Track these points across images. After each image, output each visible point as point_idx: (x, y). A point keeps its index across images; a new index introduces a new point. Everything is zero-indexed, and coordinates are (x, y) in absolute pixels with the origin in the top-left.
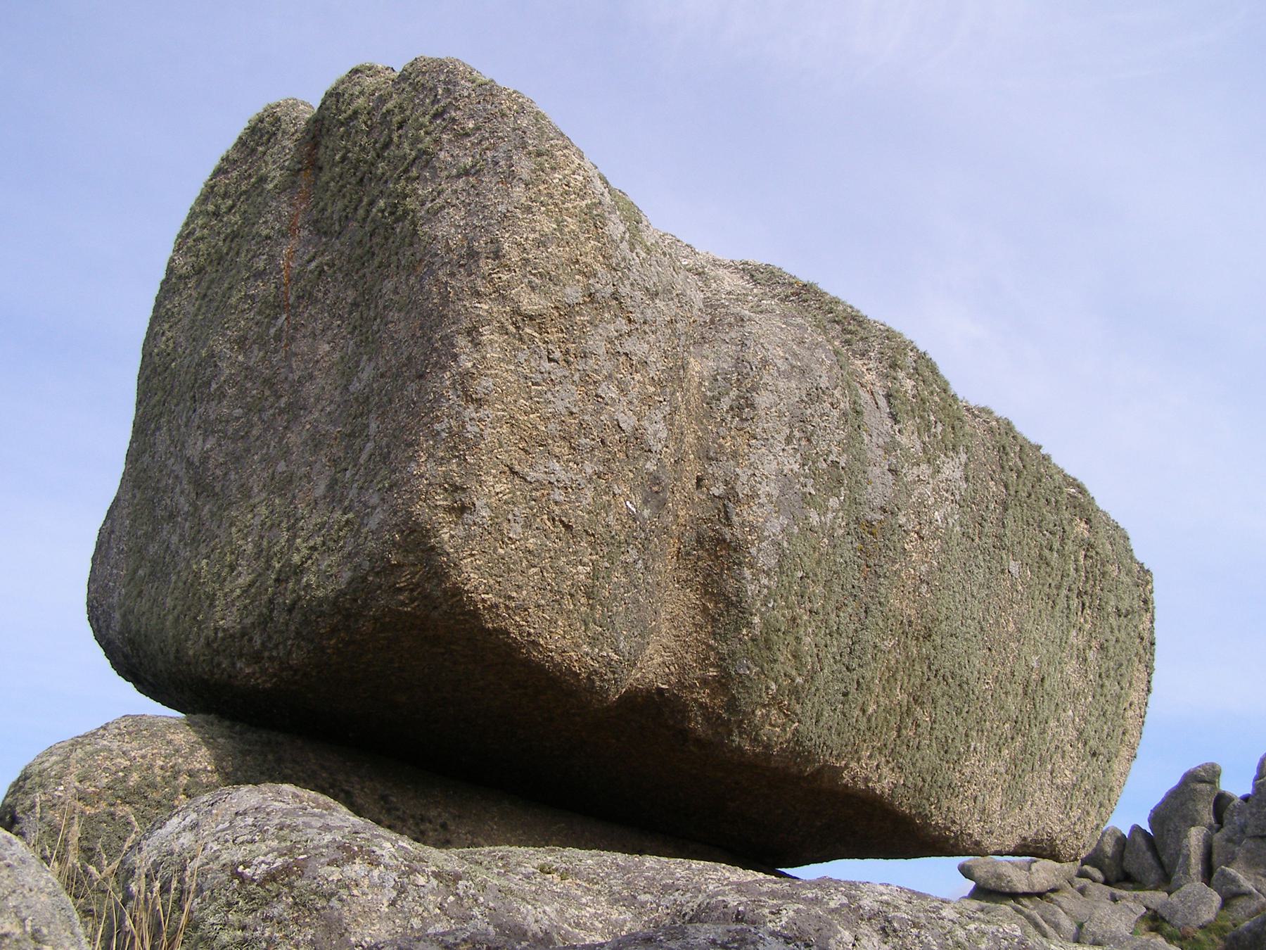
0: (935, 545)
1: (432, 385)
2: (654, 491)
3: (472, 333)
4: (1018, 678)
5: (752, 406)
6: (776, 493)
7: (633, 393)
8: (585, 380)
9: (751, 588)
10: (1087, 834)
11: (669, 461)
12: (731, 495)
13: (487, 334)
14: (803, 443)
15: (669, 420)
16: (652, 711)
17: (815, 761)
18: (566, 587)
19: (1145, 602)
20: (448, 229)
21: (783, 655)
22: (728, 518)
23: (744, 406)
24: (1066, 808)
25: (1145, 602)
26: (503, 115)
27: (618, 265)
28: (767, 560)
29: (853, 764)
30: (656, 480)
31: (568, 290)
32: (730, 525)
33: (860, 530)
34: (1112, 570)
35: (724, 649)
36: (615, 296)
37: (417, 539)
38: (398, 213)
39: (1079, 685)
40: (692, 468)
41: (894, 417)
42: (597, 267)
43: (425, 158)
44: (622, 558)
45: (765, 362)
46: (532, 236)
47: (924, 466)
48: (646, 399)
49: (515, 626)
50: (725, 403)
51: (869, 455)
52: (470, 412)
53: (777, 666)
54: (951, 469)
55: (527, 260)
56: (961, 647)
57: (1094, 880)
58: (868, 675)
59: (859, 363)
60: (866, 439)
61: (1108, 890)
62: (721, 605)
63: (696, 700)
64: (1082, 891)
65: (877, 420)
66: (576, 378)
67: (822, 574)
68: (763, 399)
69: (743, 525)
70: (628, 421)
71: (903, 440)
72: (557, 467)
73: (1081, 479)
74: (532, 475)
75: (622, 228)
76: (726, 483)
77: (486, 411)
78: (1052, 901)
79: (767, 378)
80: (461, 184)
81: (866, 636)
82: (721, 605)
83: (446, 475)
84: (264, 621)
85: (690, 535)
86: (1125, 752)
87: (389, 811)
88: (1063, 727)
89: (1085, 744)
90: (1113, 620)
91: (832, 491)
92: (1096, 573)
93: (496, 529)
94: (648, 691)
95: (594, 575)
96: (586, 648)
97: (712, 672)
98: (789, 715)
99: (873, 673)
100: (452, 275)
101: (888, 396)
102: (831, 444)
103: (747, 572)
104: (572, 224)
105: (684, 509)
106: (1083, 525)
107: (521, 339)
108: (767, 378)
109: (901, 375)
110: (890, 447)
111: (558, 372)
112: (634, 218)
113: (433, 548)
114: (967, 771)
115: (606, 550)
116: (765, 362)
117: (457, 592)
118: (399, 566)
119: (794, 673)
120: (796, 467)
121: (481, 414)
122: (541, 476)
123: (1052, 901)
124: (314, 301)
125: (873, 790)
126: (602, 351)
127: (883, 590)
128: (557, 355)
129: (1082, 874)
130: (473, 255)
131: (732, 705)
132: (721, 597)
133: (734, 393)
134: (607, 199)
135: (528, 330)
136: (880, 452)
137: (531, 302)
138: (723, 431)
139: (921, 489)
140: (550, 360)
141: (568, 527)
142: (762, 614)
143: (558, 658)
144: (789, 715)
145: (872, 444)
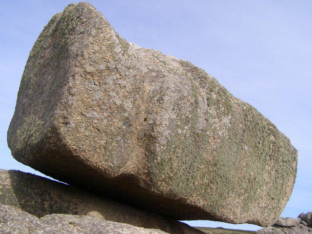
0: (219, 141)
1: (63, 90)
2: (127, 122)
3: (73, 76)
4: (246, 178)
5: (163, 100)
6: (168, 124)
7: (121, 95)
8: (105, 90)
9: (158, 149)
10: (270, 220)
11: (133, 114)
12: (154, 124)
13: (77, 77)
14: (178, 110)
15: (134, 103)
16: (128, 180)
17: (178, 197)
18: (97, 146)
19: (295, 158)
20: (74, 49)
21: (167, 168)
22: (153, 130)
23: (161, 100)
24: (262, 213)
25: (295, 158)
26: (92, 18)
27: (117, 60)
28: (163, 142)
29: (190, 198)
30: (128, 118)
31: (101, 66)
32: (153, 131)
33: (194, 135)
34: (282, 150)
35: (149, 165)
36: (116, 68)
37: (55, 130)
38: (66, 44)
39: (268, 180)
40: (143, 115)
41: (208, 105)
42: (110, 60)
43: (73, 29)
44: (116, 139)
45: (168, 88)
46: (92, 51)
47: (216, 119)
48: (125, 97)
49: (82, 155)
50: (156, 98)
51: (199, 115)
52: (70, 97)
53: (164, 171)
54: (226, 120)
55: (90, 57)
56: (226, 169)
57: (304, 225)
58: (195, 175)
59: (201, 89)
60: (199, 110)
61: (308, 228)
62: (150, 154)
63: (141, 178)
64: (301, 227)
65: (203, 106)
66: (103, 90)
67: (181, 146)
68: (166, 98)
69: (157, 132)
70: (119, 102)
71: (211, 112)
72: (96, 113)
73: (275, 124)
74: (88, 115)
75: (120, 50)
76: (154, 120)
77: (74, 97)
78: (292, 229)
79: (168, 92)
80: (80, 36)
81: (194, 164)
82: (150, 154)
83: (63, 114)
84: (26, 148)
85: (142, 134)
86: (285, 198)
87: (60, 199)
88: (263, 191)
89: (269, 196)
90: (281, 164)
91: (186, 124)
92: (277, 149)
93: (76, 129)
94: (129, 174)
95: (107, 143)
96: (103, 162)
97: (146, 171)
98: (168, 184)
99: (198, 175)
100: (72, 60)
101: (208, 99)
102: (187, 111)
103: (157, 145)
104: (104, 48)
105: (138, 126)
106: (273, 137)
107: (86, 78)
108: (168, 92)
109: (213, 93)
110: (206, 113)
111: (97, 88)
112: (126, 47)
113: (59, 133)
114: (228, 202)
115: (110, 137)
116: (168, 88)
117: (65, 145)
118: (51, 137)
119: (170, 173)
120: (175, 117)
121: (73, 98)
122: (90, 116)
123: (292, 229)
124: (50, 65)
125: (197, 205)
126: (111, 83)
127: (201, 152)
128: (97, 83)
129: (301, 223)
130: (77, 55)
131: (151, 180)
132: (149, 151)
133: (158, 96)
134: (117, 41)
135: (88, 76)
136: (203, 114)
137: (89, 69)
138: (154, 106)
139: (215, 125)
140: (95, 85)
141: (98, 130)
142: (161, 156)
143: (95, 165)
144: (168, 184)
145: (200, 112)
